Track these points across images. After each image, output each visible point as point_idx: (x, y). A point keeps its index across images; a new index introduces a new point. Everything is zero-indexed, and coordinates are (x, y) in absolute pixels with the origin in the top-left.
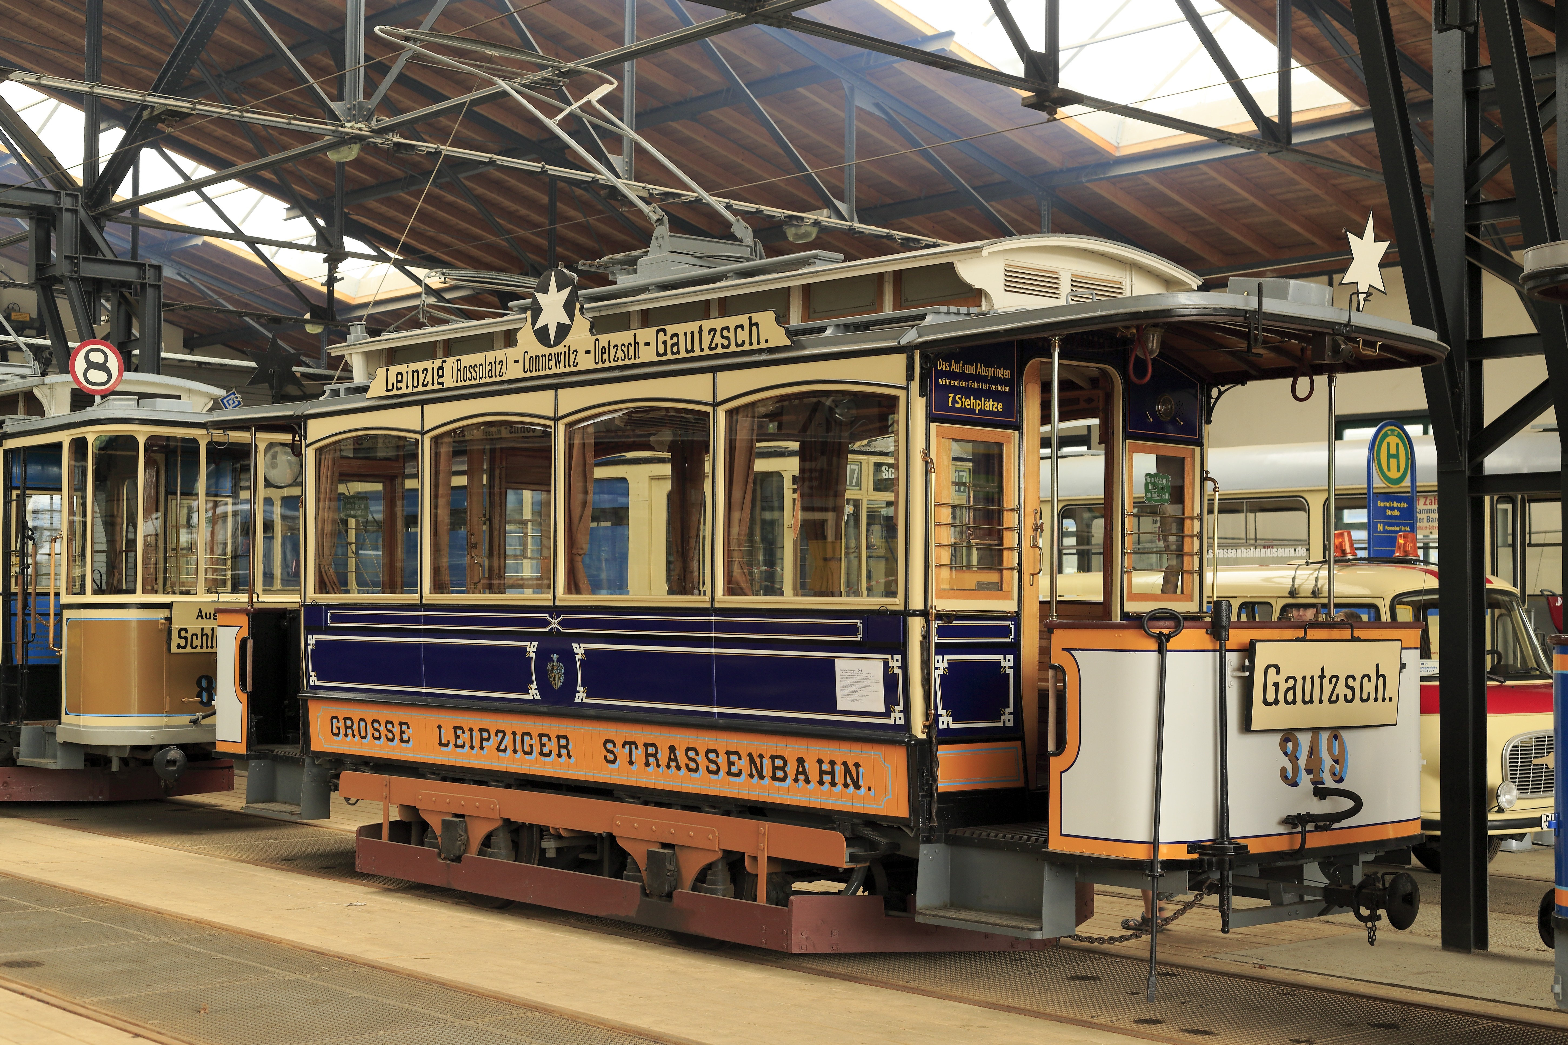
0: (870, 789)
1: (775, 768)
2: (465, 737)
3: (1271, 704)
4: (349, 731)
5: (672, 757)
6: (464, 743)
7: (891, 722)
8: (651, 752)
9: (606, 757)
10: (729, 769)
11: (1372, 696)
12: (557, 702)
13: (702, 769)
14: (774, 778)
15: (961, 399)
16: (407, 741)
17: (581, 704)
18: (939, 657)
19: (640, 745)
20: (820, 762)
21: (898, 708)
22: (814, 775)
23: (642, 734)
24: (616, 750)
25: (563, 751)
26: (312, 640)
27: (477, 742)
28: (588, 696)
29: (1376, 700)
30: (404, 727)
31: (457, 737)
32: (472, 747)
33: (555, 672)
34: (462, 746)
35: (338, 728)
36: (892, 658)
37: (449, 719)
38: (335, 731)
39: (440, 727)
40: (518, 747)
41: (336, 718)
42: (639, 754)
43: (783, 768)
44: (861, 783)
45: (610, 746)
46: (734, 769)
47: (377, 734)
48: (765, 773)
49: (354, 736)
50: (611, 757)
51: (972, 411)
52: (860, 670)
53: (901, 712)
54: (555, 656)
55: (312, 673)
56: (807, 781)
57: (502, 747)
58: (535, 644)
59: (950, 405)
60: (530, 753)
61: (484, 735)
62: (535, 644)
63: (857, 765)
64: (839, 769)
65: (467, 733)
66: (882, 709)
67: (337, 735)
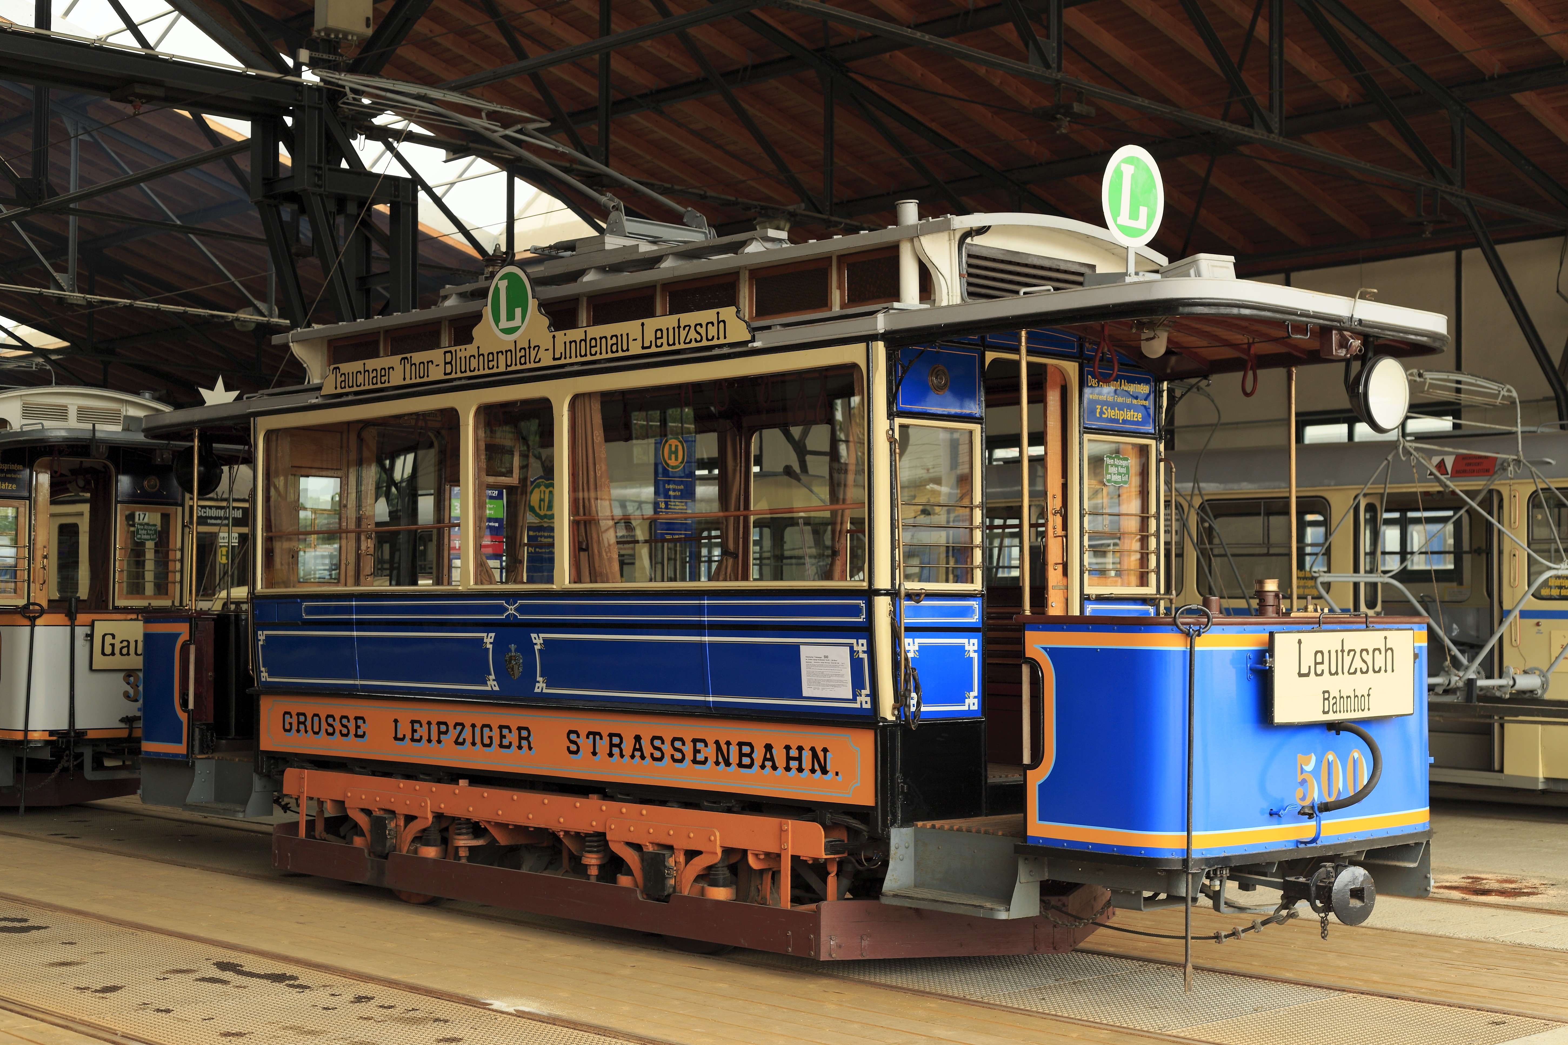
0: (837, 774)
1: (741, 755)
2: (422, 731)
3: (1333, 674)
4: (302, 727)
5: (637, 746)
6: (421, 737)
7: (858, 706)
8: (615, 743)
9: (568, 748)
10: (695, 756)
11: (1383, 669)
12: (515, 695)
13: (667, 758)
14: (740, 765)
15: (1107, 410)
16: (362, 736)
18: (910, 640)
19: (605, 735)
20: (788, 748)
21: (864, 692)
22: (781, 761)
23: (606, 724)
24: (579, 741)
25: (524, 743)
26: (262, 635)
27: (434, 737)
28: (548, 686)
29: (1386, 671)
30: (360, 722)
31: (414, 731)
32: (429, 741)
33: (513, 662)
34: (419, 741)
35: (291, 724)
36: (857, 643)
37: (406, 713)
39: (396, 721)
40: (478, 739)
41: (289, 713)
42: (603, 745)
43: (749, 755)
44: (828, 768)
45: (573, 737)
46: (700, 757)
47: (330, 730)
48: (731, 761)
49: (306, 732)
50: (573, 748)
51: (1116, 421)
52: (826, 657)
53: (867, 696)
54: (513, 647)
55: (262, 669)
56: (774, 768)
57: (461, 740)
59: (1098, 415)
60: (489, 745)
62: (493, 635)
63: (825, 750)
64: (807, 755)
65: (425, 726)
66: (850, 696)
67: (289, 731)
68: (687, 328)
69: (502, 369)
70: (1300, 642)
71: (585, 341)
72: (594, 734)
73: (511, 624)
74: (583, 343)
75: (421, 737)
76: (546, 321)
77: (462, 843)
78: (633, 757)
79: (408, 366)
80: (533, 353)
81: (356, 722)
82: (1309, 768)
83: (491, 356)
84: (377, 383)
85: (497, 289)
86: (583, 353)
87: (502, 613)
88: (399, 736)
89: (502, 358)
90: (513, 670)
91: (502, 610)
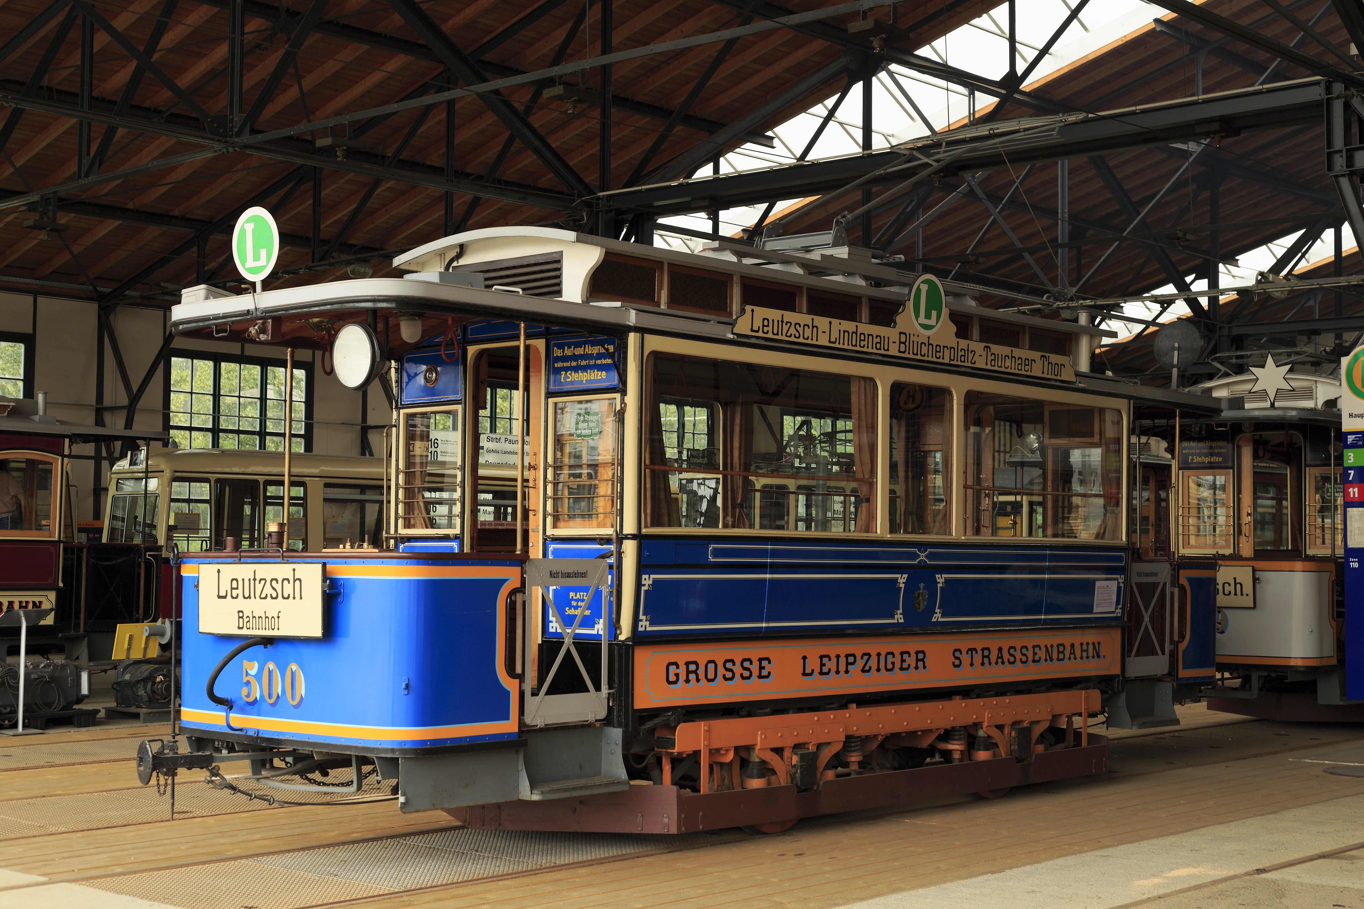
1: (1059, 652)
2: (831, 665)
6: (909, 665)
9: (953, 663)
12: (918, 624)
14: (1058, 660)
16: (767, 677)
17: (938, 623)
23: (978, 642)
27: (842, 668)
30: (764, 663)
31: (822, 665)
33: (920, 598)
34: (827, 673)
35: (893, 663)
38: (672, 678)
39: (804, 658)
40: (882, 666)
42: (978, 658)
45: (957, 654)
50: (957, 662)
54: (922, 585)
57: (867, 668)
58: (906, 576)
61: (850, 659)
62: (906, 576)
65: (834, 660)
68: (789, 324)
69: (946, 360)
70: (219, 571)
71: (856, 334)
72: (972, 650)
73: (922, 567)
74: (854, 335)
75: (1040, 658)
76: (954, 329)
77: (853, 759)
78: (997, 663)
79: (1046, 363)
80: (971, 356)
81: (1034, 650)
82: (253, 672)
83: (862, 336)
84: (767, 332)
85: (919, 290)
86: (854, 343)
87: (915, 560)
88: (807, 672)
89: (947, 352)
90: (919, 605)
91: (914, 556)
